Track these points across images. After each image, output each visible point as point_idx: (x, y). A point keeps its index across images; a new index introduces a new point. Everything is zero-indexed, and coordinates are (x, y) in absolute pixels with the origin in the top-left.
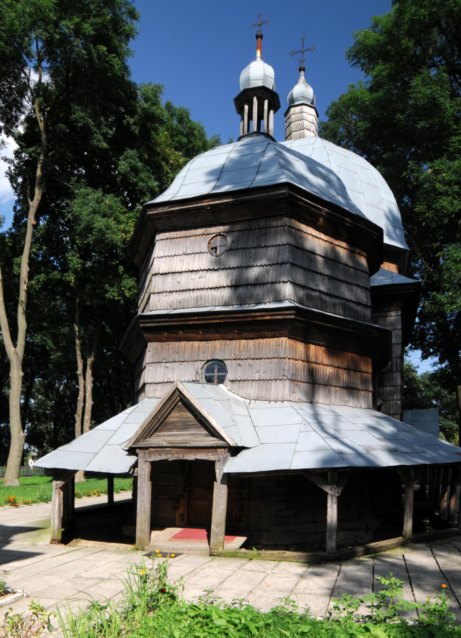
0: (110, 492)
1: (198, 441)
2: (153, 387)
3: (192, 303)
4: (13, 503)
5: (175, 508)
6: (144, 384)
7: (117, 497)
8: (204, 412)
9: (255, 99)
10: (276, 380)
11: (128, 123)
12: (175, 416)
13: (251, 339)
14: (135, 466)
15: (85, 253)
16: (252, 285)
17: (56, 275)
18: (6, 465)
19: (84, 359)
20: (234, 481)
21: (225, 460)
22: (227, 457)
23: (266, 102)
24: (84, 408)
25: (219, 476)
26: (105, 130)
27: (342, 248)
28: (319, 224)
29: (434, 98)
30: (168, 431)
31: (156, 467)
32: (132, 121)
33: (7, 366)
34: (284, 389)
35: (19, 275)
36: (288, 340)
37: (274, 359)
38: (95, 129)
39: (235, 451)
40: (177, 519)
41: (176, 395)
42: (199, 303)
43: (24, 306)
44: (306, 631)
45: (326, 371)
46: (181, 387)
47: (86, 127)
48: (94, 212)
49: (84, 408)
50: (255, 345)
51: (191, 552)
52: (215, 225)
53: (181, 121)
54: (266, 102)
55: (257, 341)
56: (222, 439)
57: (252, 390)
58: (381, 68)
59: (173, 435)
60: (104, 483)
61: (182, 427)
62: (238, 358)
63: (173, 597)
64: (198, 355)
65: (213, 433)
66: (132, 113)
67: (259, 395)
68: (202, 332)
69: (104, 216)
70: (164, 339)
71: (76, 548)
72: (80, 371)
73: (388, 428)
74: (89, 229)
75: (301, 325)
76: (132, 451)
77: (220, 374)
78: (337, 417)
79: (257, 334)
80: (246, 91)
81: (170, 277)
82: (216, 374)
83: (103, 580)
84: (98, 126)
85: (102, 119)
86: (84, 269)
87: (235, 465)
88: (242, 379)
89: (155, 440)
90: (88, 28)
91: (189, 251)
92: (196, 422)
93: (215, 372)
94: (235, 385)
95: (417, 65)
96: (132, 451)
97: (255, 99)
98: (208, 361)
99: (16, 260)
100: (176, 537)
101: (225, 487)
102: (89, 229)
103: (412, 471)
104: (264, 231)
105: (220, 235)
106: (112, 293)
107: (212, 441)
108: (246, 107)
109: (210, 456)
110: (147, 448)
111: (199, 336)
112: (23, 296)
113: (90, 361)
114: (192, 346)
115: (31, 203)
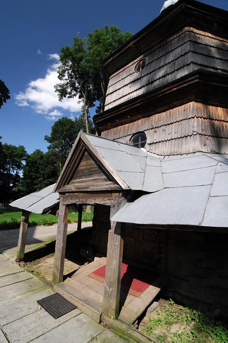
1: (96, 186)
10: (186, 137)
13: (164, 111)
21: (119, 205)
22: (121, 203)
25: (113, 225)
30: (79, 179)
34: (194, 144)
36: (195, 103)
37: (183, 121)
39: (132, 195)
41: (81, 146)
61: (88, 174)
62: (154, 127)
64: (128, 132)
67: (172, 151)
68: (130, 116)
70: (109, 128)
77: (142, 142)
79: (168, 106)
81: (114, 94)
82: (140, 142)
88: (158, 141)
111: (128, 119)
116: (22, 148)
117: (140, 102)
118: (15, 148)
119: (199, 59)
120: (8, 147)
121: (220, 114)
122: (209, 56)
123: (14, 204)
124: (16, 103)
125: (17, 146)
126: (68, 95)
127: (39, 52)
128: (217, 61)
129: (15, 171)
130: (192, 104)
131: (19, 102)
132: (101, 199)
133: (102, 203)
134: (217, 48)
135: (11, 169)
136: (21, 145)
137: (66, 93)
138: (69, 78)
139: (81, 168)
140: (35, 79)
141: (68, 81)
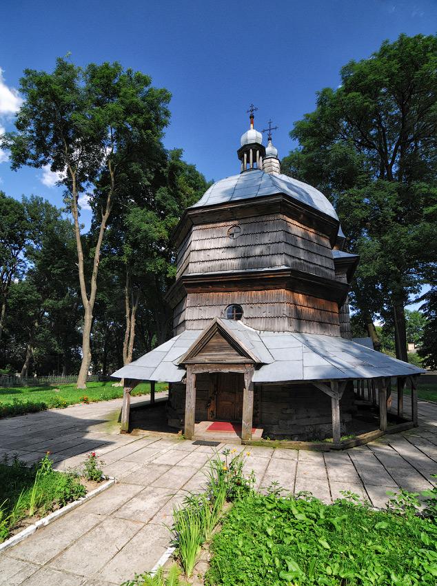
0: (153, 392)
2: (191, 323)
3: (217, 268)
4: (86, 401)
5: (207, 407)
6: (185, 321)
7: (158, 396)
8: (237, 339)
9: (251, 150)
11: (163, 172)
12: (214, 341)
14: (185, 377)
15: (135, 245)
16: (259, 256)
17: (116, 258)
18: (78, 374)
19: (131, 307)
20: (259, 388)
21: (252, 373)
23: (258, 152)
24: (129, 338)
25: (247, 384)
26: (149, 175)
27: (312, 233)
28: (300, 218)
29: (346, 154)
31: (199, 378)
32: (165, 170)
33: (83, 311)
34: (285, 324)
35: (93, 259)
38: (143, 175)
39: (258, 366)
40: (209, 415)
42: (223, 268)
43: (96, 275)
44: (383, 527)
45: (309, 311)
46: (219, 321)
47: (139, 174)
48: (142, 220)
49: (129, 338)
50: (262, 294)
51: (227, 441)
52: (232, 220)
53: (190, 172)
54: (258, 152)
55: (263, 292)
56: (249, 357)
57: (261, 324)
58: (310, 141)
59: (212, 355)
60: (149, 386)
63: (247, 489)
65: (242, 353)
66: (165, 166)
69: (147, 223)
71: (138, 438)
72: (127, 315)
73: (356, 351)
74: (138, 230)
75: (294, 280)
76: (181, 366)
78: (321, 343)
80: (245, 146)
83: (171, 466)
84: (145, 173)
85: (148, 170)
86: (133, 254)
87: (259, 377)
89: (199, 359)
90: (141, 121)
91: (215, 236)
92: (229, 346)
93: (236, 312)
94: (249, 321)
95: (329, 138)
96: (181, 366)
97: (251, 150)
98: (229, 305)
99: (92, 250)
100: (211, 429)
101: (252, 392)
102: (138, 230)
103: (383, 380)
104: (265, 223)
105: (235, 226)
106: (150, 267)
107: (241, 359)
108: (245, 155)
109: (241, 370)
110: (194, 364)
112: (95, 270)
113: (134, 309)
114: (218, 296)
115: (103, 217)
123: (114, 375)
126: (29, 161)
128: (301, 251)
132: (235, 369)
133: (236, 371)
137: (26, 156)
139: (210, 344)
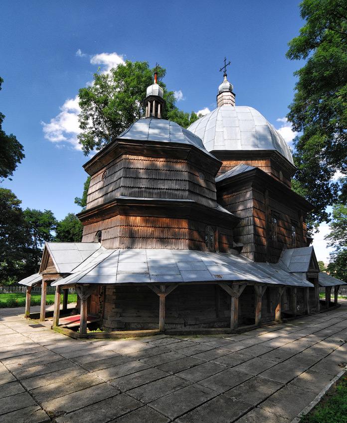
116: (49, 214)
117: (97, 210)
118: (40, 214)
119: (129, 183)
120: (31, 214)
121: (137, 222)
122: (137, 178)
124: (47, 137)
125: (43, 211)
127: (79, 52)
129: (43, 245)
130: (119, 217)
131: (52, 135)
134: (147, 169)
135: (38, 242)
136: (48, 210)
138: (94, 125)
140: (100, 53)
141: (94, 129)
